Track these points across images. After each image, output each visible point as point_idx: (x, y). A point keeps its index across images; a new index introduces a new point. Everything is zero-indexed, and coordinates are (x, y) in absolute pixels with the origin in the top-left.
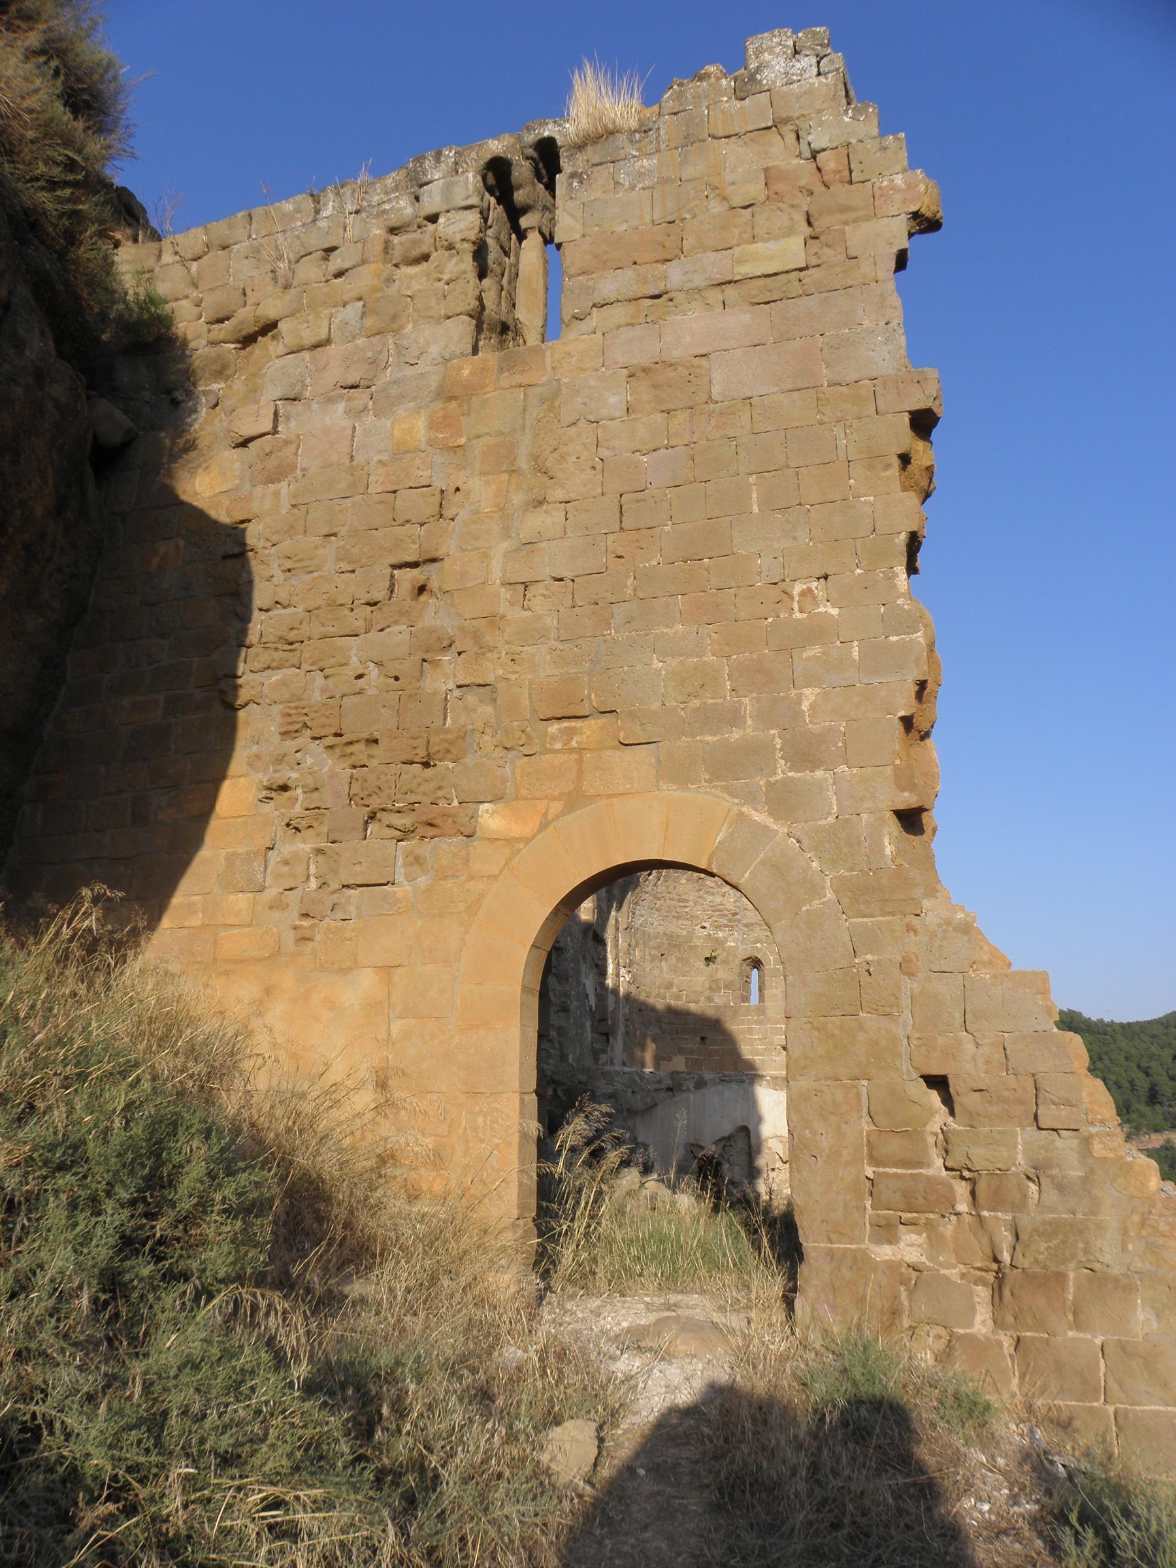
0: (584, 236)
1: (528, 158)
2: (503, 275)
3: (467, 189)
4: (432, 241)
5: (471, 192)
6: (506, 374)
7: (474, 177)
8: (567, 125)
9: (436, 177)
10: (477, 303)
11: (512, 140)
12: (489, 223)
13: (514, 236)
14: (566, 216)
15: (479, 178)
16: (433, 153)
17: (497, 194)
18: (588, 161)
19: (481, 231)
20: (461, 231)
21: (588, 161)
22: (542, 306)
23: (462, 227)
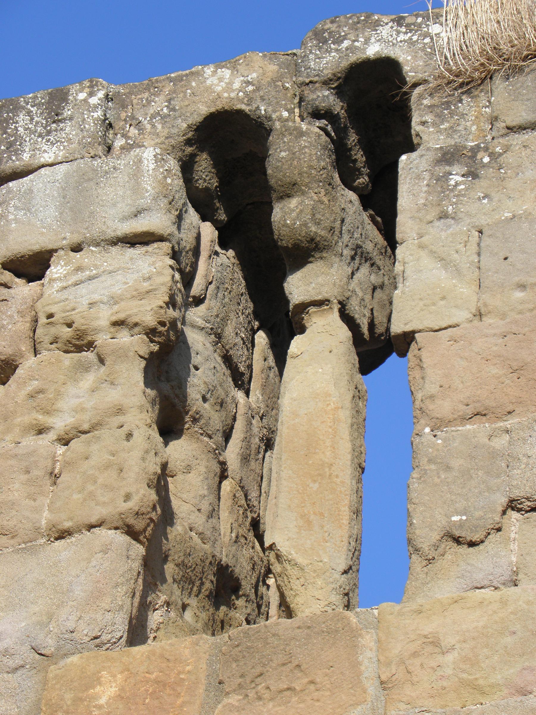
0: (479, 315)
1: (316, 114)
2: (227, 436)
3: (137, 190)
4: (24, 326)
5: (146, 201)
6: (234, 699)
7: (159, 160)
8: (435, 29)
9: (48, 158)
10: (153, 496)
11: (272, 68)
12: (197, 288)
13: (261, 338)
14: (426, 261)
15: (173, 165)
16: (41, 96)
17: (223, 216)
18: (494, 120)
19: (172, 303)
20: (114, 300)
21: (494, 120)
22: (346, 513)
23: (117, 289)
